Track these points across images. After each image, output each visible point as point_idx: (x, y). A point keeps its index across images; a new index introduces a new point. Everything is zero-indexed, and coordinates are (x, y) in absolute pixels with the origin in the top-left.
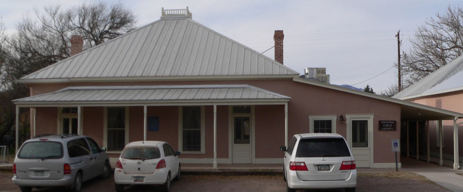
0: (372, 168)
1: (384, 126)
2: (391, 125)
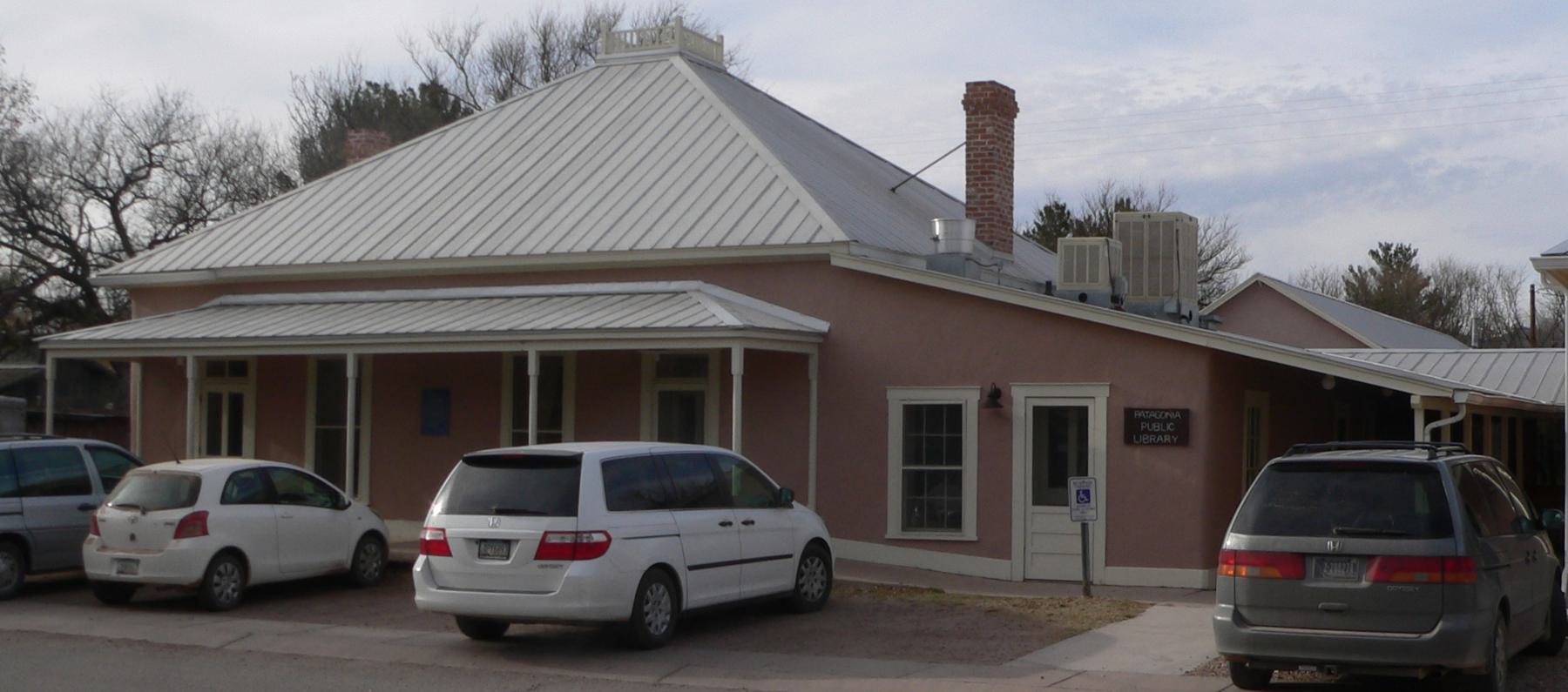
0: (1098, 583)
1: (1142, 427)
2: (1168, 428)
